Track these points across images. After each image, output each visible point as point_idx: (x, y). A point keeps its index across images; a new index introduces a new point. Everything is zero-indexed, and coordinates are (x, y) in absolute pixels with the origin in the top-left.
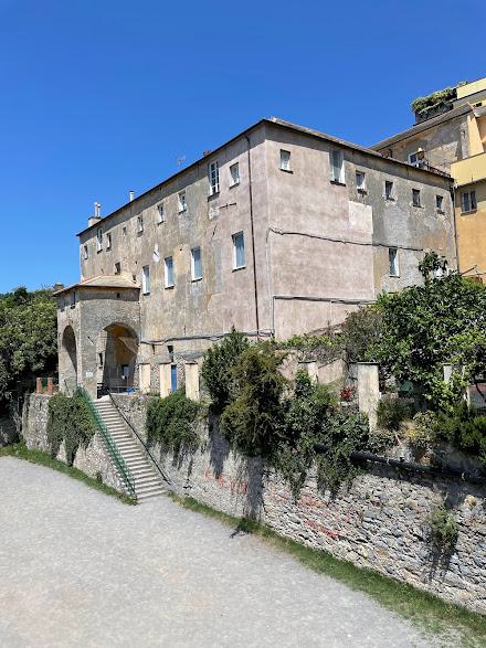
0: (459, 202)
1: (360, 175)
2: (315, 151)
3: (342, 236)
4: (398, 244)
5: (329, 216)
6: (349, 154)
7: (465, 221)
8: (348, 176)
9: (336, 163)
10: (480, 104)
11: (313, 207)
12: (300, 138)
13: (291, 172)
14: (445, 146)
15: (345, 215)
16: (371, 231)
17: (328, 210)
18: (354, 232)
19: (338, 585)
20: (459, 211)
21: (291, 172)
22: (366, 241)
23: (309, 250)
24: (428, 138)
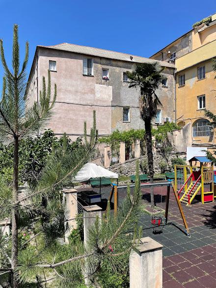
0: (178, 81)
1: (105, 71)
2: (73, 60)
3: (89, 102)
4: (131, 105)
5: (80, 92)
6: (98, 60)
7: (180, 91)
8: (96, 71)
9: (89, 66)
10: (210, 21)
11: (70, 88)
12: (54, 53)
13: (56, 72)
14: (184, 49)
15: (92, 91)
16: (111, 99)
17: (80, 89)
18: (98, 100)
19: (141, 281)
20: (178, 85)
21: (56, 72)
22: (108, 105)
23: (66, 110)
24: (177, 46)
